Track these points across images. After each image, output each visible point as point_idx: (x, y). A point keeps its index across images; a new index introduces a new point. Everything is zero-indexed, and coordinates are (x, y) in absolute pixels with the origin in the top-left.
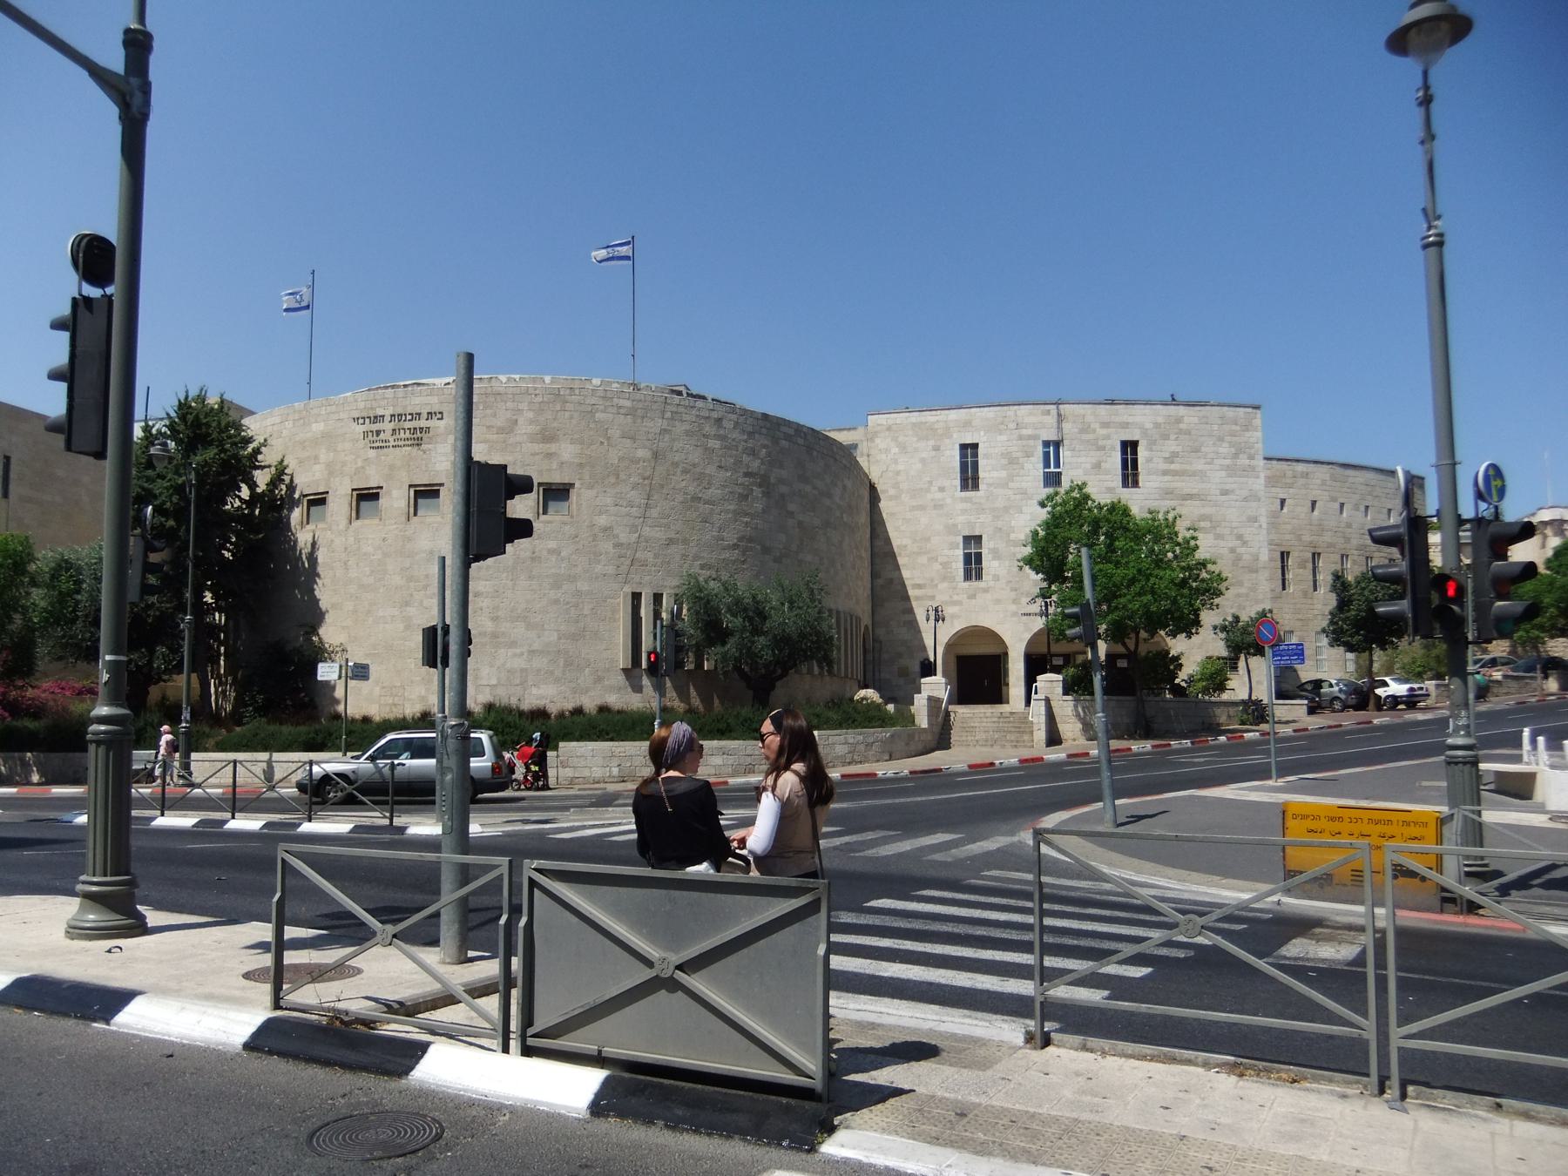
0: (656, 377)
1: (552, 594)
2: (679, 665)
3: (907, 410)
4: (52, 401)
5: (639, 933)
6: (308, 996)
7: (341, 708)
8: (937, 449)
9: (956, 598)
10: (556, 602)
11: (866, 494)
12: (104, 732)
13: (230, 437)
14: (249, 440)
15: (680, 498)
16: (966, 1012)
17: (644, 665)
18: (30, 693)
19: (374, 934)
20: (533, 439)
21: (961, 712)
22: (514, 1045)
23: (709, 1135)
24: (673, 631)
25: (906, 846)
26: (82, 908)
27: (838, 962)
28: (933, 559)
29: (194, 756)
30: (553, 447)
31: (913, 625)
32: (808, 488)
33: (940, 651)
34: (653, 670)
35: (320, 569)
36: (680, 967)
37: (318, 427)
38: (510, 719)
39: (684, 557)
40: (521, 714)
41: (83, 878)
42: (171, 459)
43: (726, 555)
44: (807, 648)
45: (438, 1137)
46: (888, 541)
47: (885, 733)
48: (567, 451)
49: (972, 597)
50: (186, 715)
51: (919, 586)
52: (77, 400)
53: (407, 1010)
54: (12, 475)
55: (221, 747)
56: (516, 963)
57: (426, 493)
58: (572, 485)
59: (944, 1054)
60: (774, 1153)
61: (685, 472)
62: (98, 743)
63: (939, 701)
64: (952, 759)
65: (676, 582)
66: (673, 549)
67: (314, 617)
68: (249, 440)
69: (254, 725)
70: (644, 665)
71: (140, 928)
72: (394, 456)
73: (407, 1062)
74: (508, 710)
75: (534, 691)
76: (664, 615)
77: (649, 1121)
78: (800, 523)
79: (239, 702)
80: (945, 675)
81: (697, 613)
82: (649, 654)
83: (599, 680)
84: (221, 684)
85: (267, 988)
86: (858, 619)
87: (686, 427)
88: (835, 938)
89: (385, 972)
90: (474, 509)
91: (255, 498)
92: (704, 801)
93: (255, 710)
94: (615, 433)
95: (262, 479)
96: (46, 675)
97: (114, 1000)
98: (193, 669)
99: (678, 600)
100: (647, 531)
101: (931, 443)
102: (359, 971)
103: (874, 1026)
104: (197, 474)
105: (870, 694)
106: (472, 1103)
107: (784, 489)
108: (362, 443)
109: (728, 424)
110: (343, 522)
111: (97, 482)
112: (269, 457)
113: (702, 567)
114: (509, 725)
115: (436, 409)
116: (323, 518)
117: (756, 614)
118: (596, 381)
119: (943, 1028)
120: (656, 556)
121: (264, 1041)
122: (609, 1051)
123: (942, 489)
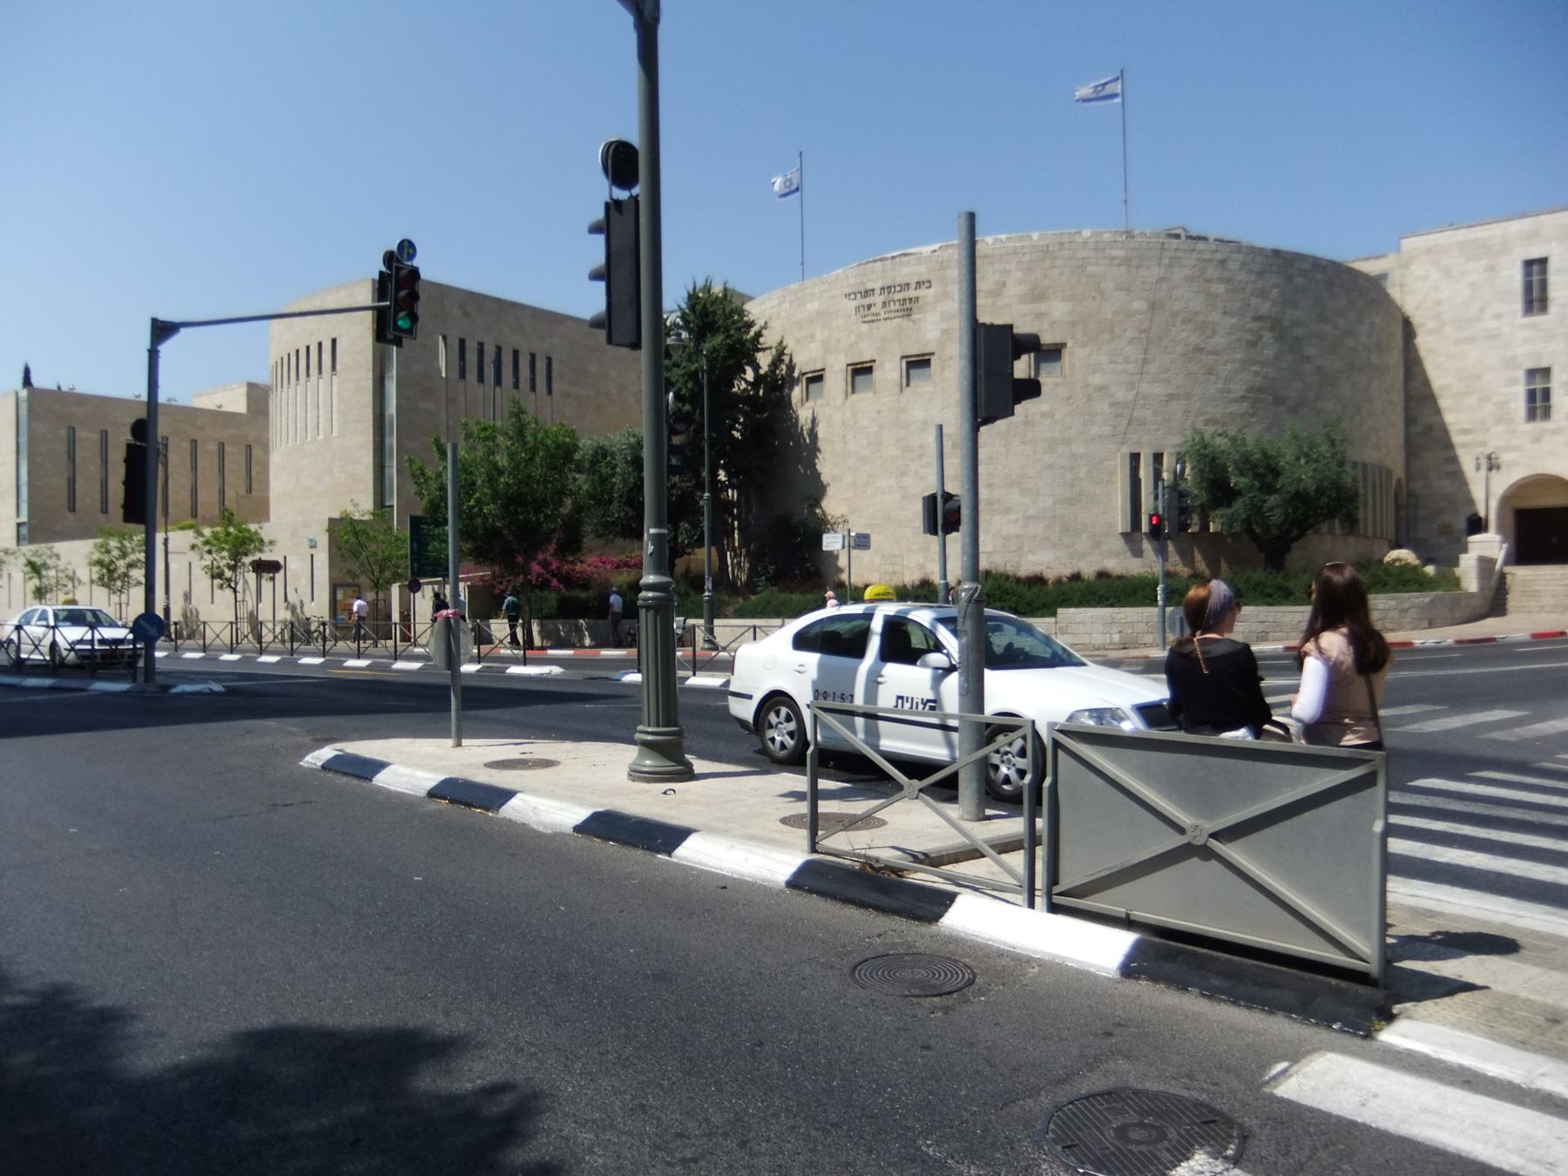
0: (1150, 221)
1: (1047, 459)
2: (1183, 527)
3: (1453, 226)
4: (590, 301)
5: (1168, 797)
6: (840, 841)
7: (844, 577)
8: (1491, 269)
9: (1514, 442)
10: (1051, 466)
11: (1398, 329)
12: (652, 599)
13: (734, 322)
14: (750, 325)
15: (1180, 349)
16: (1549, 908)
17: (1145, 528)
18: (579, 567)
19: (900, 787)
20: (1023, 299)
21: (1521, 575)
22: (1040, 901)
23: (1249, 1008)
24: (1177, 492)
25: (1456, 722)
26: (640, 755)
27: (1397, 846)
28: (1486, 399)
29: (717, 622)
30: (1043, 307)
31: (1457, 476)
32: (1328, 328)
33: (1494, 504)
34: (1156, 533)
35: (820, 444)
36: (1214, 836)
37: (813, 306)
38: (1007, 585)
39: (1186, 412)
40: (1018, 580)
41: (640, 728)
42: (685, 347)
43: (1234, 408)
44: (1331, 503)
45: (971, 982)
46: (1426, 382)
47: (1424, 598)
48: (1059, 309)
49: (1537, 439)
50: (708, 585)
51: (1466, 432)
52: (615, 297)
53: (933, 861)
54: (554, 374)
55: (740, 614)
56: (1041, 823)
57: (918, 363)
58: (1064, 345)
59: (1523, 952)
60: (1323, 1034)
61: (1186, 321)
62: (648, 608)
63: (1492, 561)
64: (1512, 627)
65: (1177, 440)
66: (1174, 405)
67: (816, 490)
68: (750, 325)
69: (768, 593)
70: (1145, 528)
71: (688, 775)
72: (887, 328)
73: (936, 909)
74: (1006, 577)
75: (1031, 557)
76: (1165, 475)
77: (1183, 987)
78: (1319, 369)
79: (753, 573)
80: (1501, 529)
81: (1202, 471)
82: (1151, 516)
83: (1097, 545)
84: (736, 555)
85: (804, 833)
86: (1389, 473)
87: (1187, 272)
88: (1395, 819)
89: (908, 826)
90: (981, 372)
91: (759, 380)
92: (1244, 666)
93: (768, 580)
94: (1108, 285)
95: (764, 360)
96: (590, 551)
97: (672, 836)
98: (712, 543)
99: (1180, 458)
100: (1145, 388)
101: (1484, 263)
102: (884, 823)
103: (1432, 914)
104: (708, 361)
105: (1405, 555)
106: (1001, 954)
107: (1300, 332)
108: (854, 318)
109: (1234, 266)
110: (840, 397)
111: (633, 372)
112: (769, 339)
113: (1207, 423)
114: (1006, 591)
115: (924, 277)
116: (821, 395)
117: (1266, 472)
118: (1086, 233)
119: (1520, 923)
120: (1155, 414)
121: (808, 879)
122: (1138, 914)
123: (1498, 316)
